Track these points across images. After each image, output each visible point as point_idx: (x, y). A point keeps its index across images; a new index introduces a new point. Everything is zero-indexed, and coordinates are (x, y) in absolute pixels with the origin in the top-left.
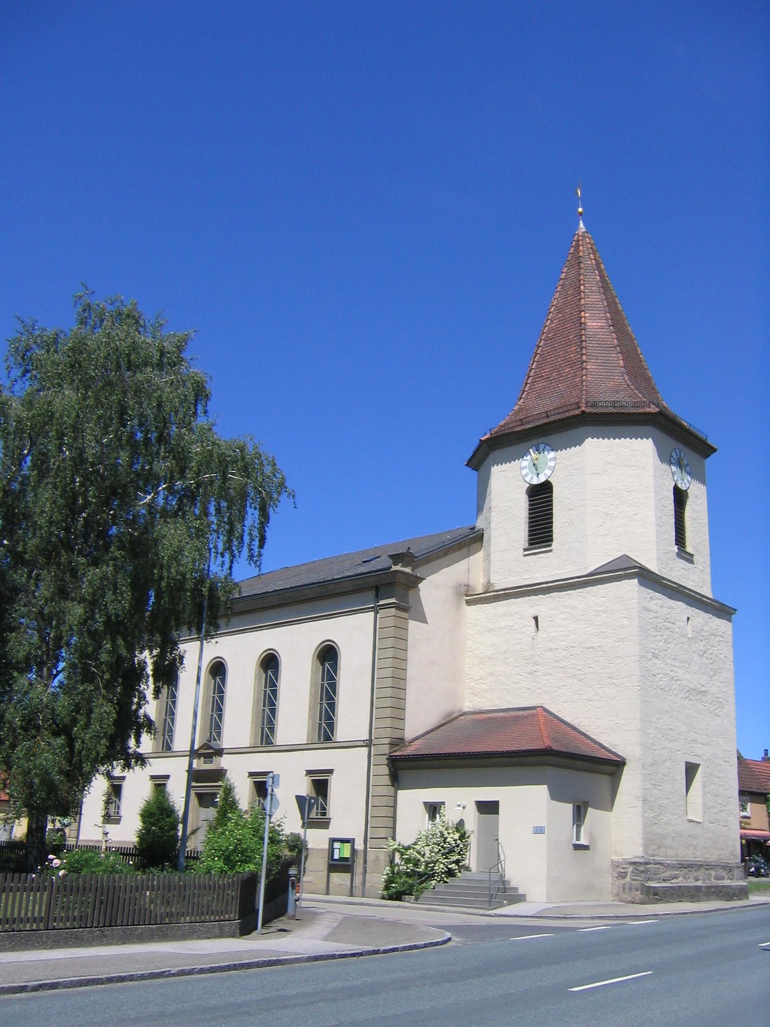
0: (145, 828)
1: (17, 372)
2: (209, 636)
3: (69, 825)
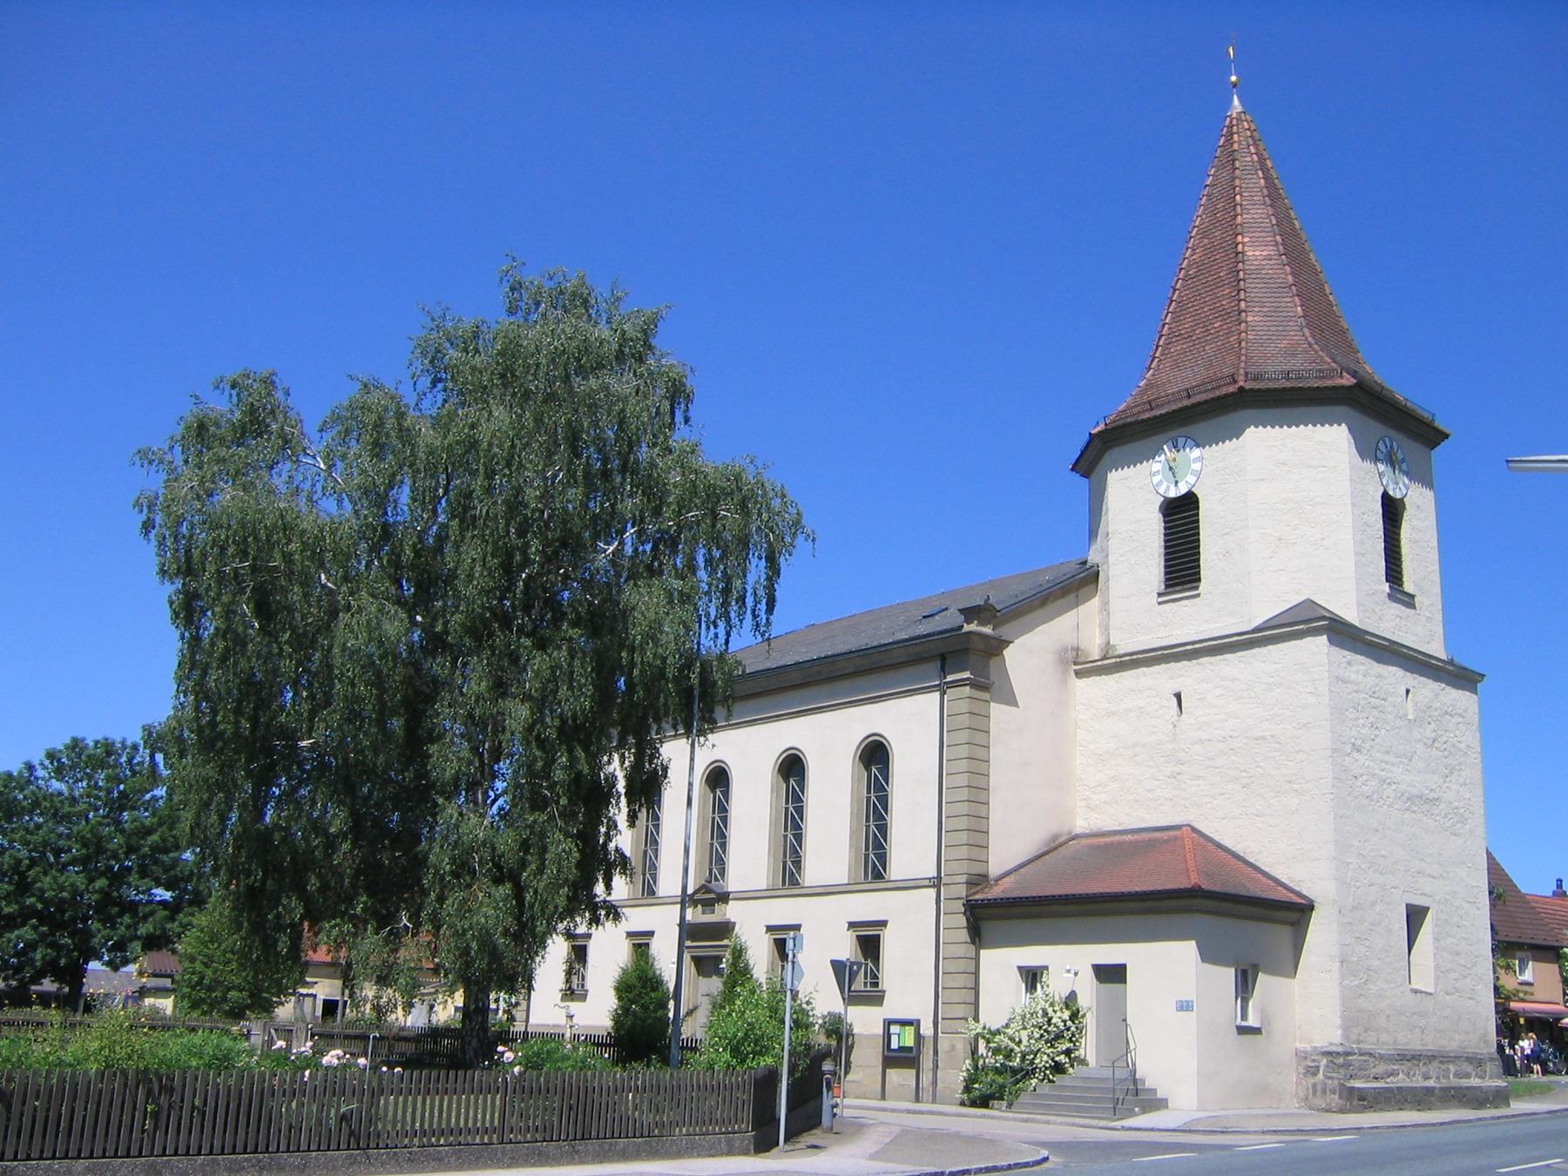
0: (622, 1007)
1: (425, 382)
2: (702, 733)
3: (517, 1004)
